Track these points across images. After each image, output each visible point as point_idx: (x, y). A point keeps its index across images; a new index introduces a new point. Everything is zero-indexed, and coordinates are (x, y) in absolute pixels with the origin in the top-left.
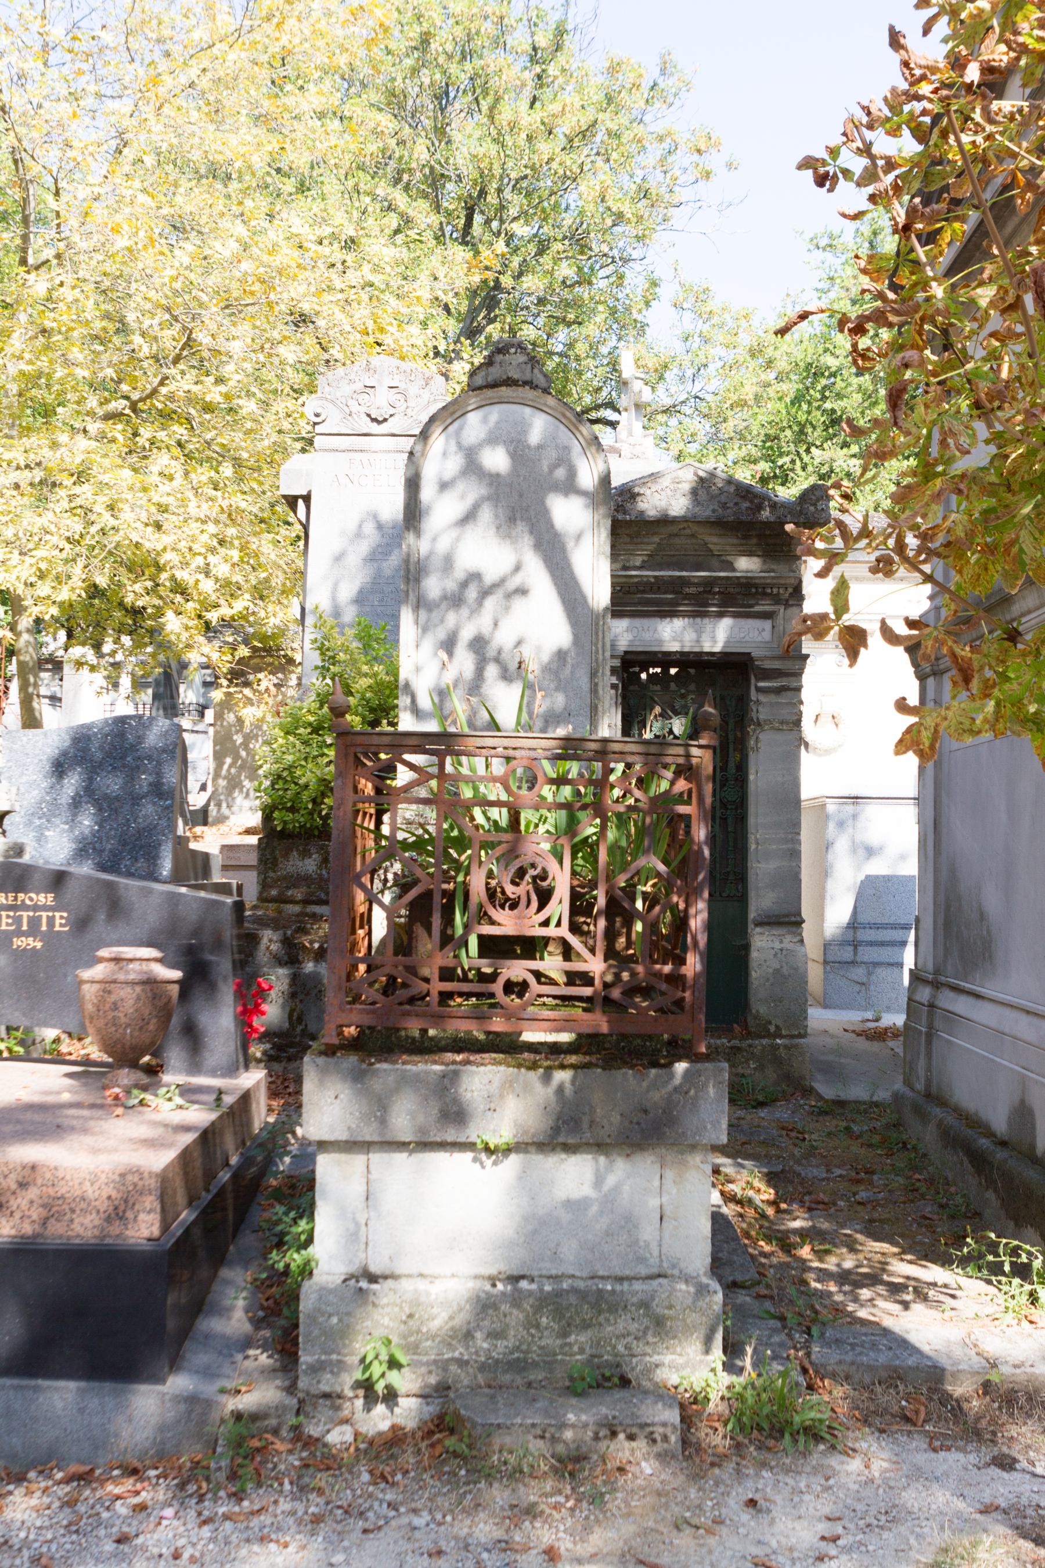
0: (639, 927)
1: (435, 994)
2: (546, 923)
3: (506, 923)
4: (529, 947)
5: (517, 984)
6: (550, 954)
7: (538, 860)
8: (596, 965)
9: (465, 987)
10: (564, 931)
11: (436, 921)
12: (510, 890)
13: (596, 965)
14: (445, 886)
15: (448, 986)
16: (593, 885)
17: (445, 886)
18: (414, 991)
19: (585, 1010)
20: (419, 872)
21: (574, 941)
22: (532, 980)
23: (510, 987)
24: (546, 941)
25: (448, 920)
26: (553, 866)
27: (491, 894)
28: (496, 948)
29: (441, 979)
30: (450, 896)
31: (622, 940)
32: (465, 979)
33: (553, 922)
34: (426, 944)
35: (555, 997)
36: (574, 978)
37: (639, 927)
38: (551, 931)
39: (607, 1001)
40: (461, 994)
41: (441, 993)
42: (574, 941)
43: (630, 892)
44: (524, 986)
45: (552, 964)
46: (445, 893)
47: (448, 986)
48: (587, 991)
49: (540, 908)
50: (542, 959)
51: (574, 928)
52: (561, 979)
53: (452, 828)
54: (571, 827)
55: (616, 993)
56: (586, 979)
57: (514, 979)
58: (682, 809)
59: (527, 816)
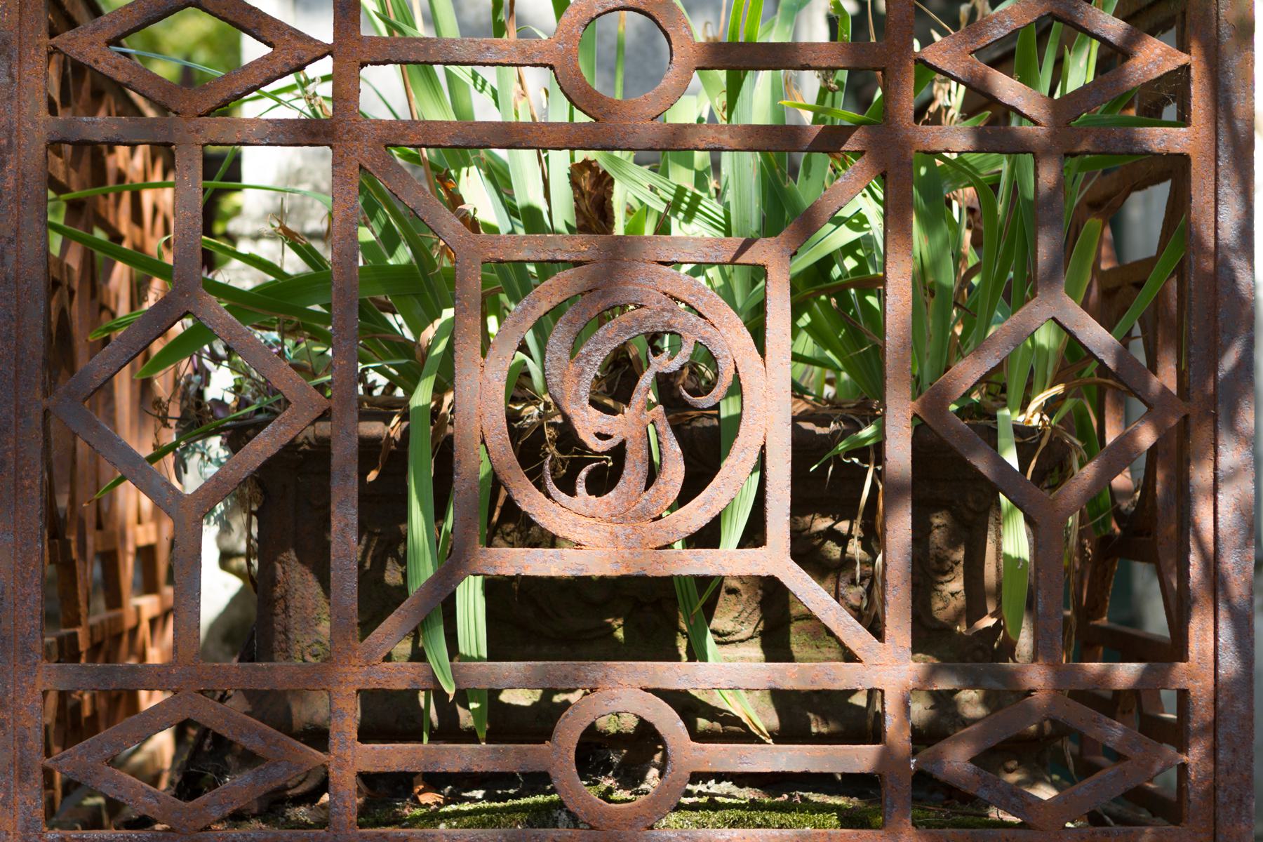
0: (1015, 539)
1: (346, 795)
2: (708, 537)
3: (586, 539)
4: (653, 614)
5: (619, 739)
6: (723, 639)
7: (683, 320)
8: (889, 670)
9: (457, 757)
10: (774, 560)
11: (344, 519)
12: (589, 424)
13: (889, 670)
14: (374, 429)
15: (393, 756)
16: (867, 408)
17: (374, 429)
18: (278, 776)
19: (849, 820)
20: (288, 383)
21: (808, 591)
22: (668, 721)
23: (595, 751)
24: (709, 590)
25: (385, 534)
26: (732, 340)
27: (528, 447)
28: (543, 619)
29: (366, 735)
30: (389, 460)
31: (955, 585)
32: (450, 732)
33: (733, 531)
34: (316, 615)
35: (741, 779)
36: (798, 714)
37: (1015, 539)
38: (729, 560)
39: (932, 792)
40: (434, 781)
41: (366, 778)
42: (808, 591)
43: (981, 419)
44: (645, 739)
45: (732, 672)
46: (369, 450)
47: (393, 756)
48: (859, 758)
49: (693, 486)
50: (697, 654)
51: (805, 551)
52: (763, 717)
53: (389, 240)
54: (785, 215)
55: (957, 758)
56: (858, 723)
57: (608, 725)
58: (1163, 138)
59: (633, 188)
